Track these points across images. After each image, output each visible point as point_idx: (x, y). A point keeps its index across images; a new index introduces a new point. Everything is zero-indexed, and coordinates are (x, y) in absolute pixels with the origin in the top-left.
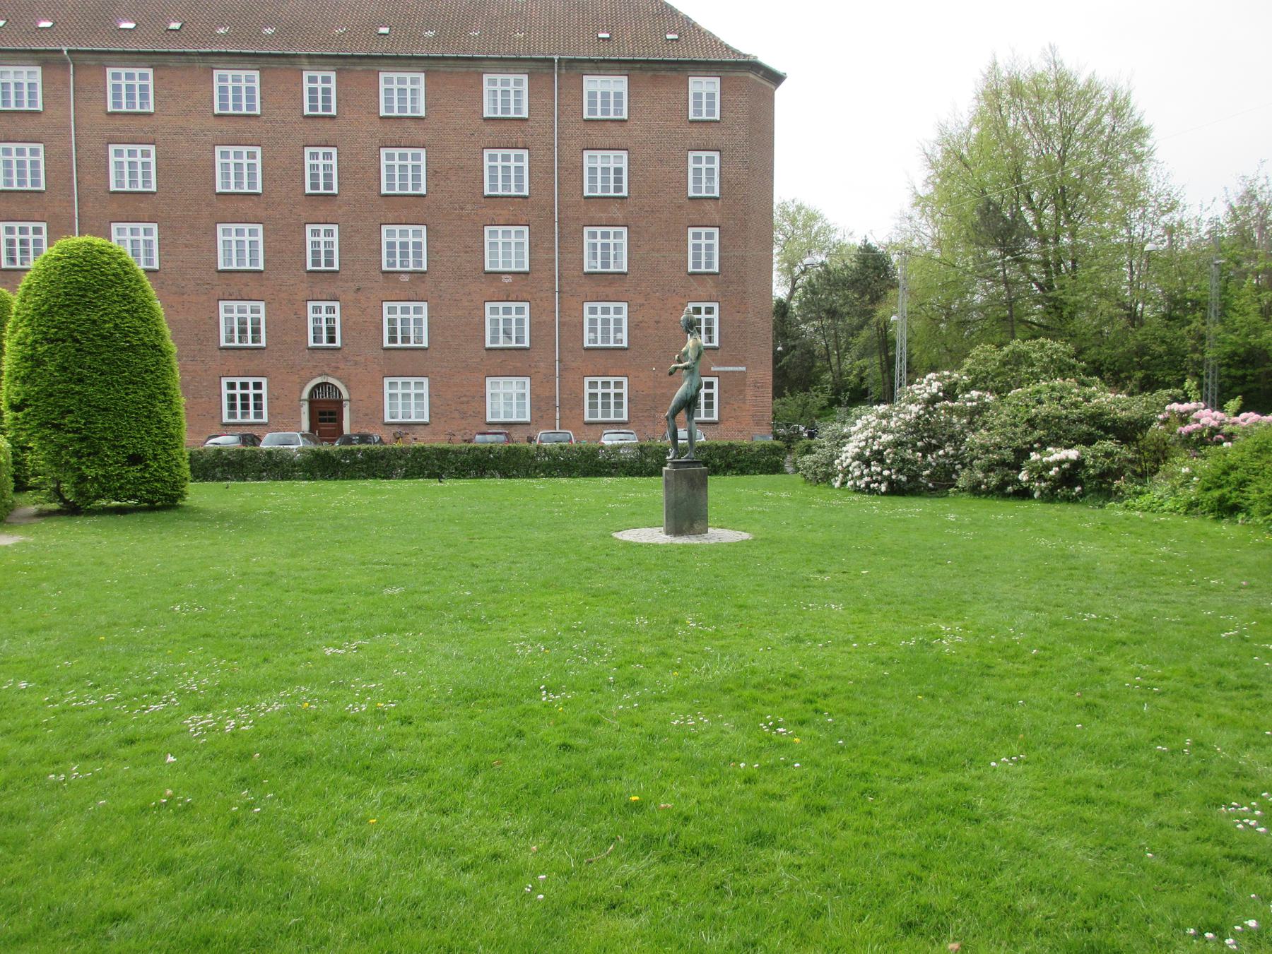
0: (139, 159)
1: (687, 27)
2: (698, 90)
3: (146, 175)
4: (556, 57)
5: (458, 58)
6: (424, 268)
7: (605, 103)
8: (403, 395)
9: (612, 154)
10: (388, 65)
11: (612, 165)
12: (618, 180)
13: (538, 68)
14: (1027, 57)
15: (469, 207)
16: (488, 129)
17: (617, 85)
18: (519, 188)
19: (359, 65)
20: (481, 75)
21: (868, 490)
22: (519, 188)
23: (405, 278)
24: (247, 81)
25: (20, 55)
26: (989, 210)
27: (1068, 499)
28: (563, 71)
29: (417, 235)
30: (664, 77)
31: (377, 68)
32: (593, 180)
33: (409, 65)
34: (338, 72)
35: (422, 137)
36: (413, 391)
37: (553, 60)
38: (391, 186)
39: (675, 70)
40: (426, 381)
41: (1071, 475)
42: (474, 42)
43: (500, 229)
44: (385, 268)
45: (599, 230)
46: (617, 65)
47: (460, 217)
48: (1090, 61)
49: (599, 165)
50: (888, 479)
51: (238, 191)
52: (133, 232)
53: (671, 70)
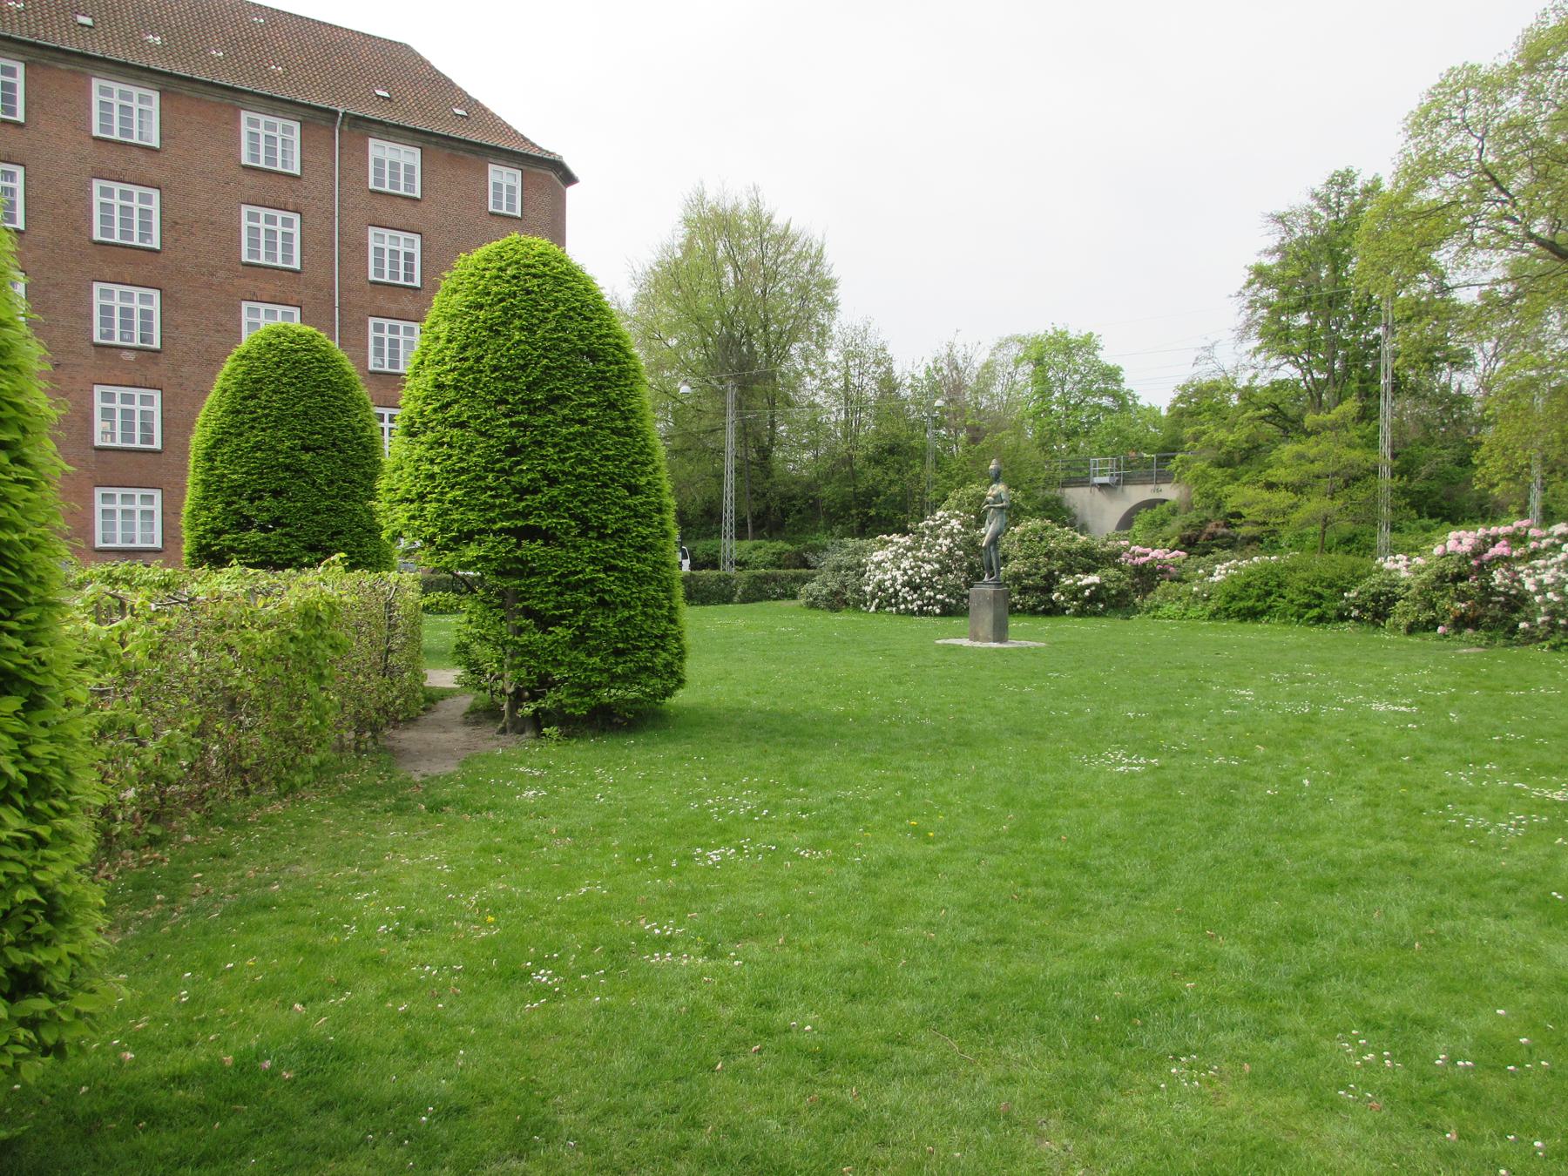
0: (279, 228)
1: (476, 111)
2: (498, 180)
3: (288, 248)
4: (341, 110)
5: (212, 84)
6: (157, 345)
7: (394, 176)
8: (124, 512)
9: (402, 235)
10: (106, 71)
11: (402, 249)
12: (409, 268)
13: (315, 119)
14: (730, 188)
15: (222, 274)
16: (248, 180)
17: (408, 156)
18: (288, 258)
19: (62, 61)
20: (237, 110)
21: (921, 612)
22: (288, 258)
23: (131, 356)
24: (141, 101)
25: (99, 64)
26: (729, 344)
27: (1095, 614)
28: (346, 128)
29: (146, 303)
30: (44, 66)
31: (89, 71)
32: (379, 262)
33: (139, 78)
34: (28, 65)
35: (155, 174)
36: (138, 506)
37: (336, 113)
38: (107, 231)
39: (474, 153)
40: (157, 494)
41: (1098, 594)
42: (81, 28)
43: (263, 307)
44: (97, 339)
45: (387, 323)
46: (411, 134)
47: (210, 286)
48: (790, 209)
49: (387, 246)
50: (942, 602)
51: (269, 263)
52: (123, 296)
53: (470, 152)
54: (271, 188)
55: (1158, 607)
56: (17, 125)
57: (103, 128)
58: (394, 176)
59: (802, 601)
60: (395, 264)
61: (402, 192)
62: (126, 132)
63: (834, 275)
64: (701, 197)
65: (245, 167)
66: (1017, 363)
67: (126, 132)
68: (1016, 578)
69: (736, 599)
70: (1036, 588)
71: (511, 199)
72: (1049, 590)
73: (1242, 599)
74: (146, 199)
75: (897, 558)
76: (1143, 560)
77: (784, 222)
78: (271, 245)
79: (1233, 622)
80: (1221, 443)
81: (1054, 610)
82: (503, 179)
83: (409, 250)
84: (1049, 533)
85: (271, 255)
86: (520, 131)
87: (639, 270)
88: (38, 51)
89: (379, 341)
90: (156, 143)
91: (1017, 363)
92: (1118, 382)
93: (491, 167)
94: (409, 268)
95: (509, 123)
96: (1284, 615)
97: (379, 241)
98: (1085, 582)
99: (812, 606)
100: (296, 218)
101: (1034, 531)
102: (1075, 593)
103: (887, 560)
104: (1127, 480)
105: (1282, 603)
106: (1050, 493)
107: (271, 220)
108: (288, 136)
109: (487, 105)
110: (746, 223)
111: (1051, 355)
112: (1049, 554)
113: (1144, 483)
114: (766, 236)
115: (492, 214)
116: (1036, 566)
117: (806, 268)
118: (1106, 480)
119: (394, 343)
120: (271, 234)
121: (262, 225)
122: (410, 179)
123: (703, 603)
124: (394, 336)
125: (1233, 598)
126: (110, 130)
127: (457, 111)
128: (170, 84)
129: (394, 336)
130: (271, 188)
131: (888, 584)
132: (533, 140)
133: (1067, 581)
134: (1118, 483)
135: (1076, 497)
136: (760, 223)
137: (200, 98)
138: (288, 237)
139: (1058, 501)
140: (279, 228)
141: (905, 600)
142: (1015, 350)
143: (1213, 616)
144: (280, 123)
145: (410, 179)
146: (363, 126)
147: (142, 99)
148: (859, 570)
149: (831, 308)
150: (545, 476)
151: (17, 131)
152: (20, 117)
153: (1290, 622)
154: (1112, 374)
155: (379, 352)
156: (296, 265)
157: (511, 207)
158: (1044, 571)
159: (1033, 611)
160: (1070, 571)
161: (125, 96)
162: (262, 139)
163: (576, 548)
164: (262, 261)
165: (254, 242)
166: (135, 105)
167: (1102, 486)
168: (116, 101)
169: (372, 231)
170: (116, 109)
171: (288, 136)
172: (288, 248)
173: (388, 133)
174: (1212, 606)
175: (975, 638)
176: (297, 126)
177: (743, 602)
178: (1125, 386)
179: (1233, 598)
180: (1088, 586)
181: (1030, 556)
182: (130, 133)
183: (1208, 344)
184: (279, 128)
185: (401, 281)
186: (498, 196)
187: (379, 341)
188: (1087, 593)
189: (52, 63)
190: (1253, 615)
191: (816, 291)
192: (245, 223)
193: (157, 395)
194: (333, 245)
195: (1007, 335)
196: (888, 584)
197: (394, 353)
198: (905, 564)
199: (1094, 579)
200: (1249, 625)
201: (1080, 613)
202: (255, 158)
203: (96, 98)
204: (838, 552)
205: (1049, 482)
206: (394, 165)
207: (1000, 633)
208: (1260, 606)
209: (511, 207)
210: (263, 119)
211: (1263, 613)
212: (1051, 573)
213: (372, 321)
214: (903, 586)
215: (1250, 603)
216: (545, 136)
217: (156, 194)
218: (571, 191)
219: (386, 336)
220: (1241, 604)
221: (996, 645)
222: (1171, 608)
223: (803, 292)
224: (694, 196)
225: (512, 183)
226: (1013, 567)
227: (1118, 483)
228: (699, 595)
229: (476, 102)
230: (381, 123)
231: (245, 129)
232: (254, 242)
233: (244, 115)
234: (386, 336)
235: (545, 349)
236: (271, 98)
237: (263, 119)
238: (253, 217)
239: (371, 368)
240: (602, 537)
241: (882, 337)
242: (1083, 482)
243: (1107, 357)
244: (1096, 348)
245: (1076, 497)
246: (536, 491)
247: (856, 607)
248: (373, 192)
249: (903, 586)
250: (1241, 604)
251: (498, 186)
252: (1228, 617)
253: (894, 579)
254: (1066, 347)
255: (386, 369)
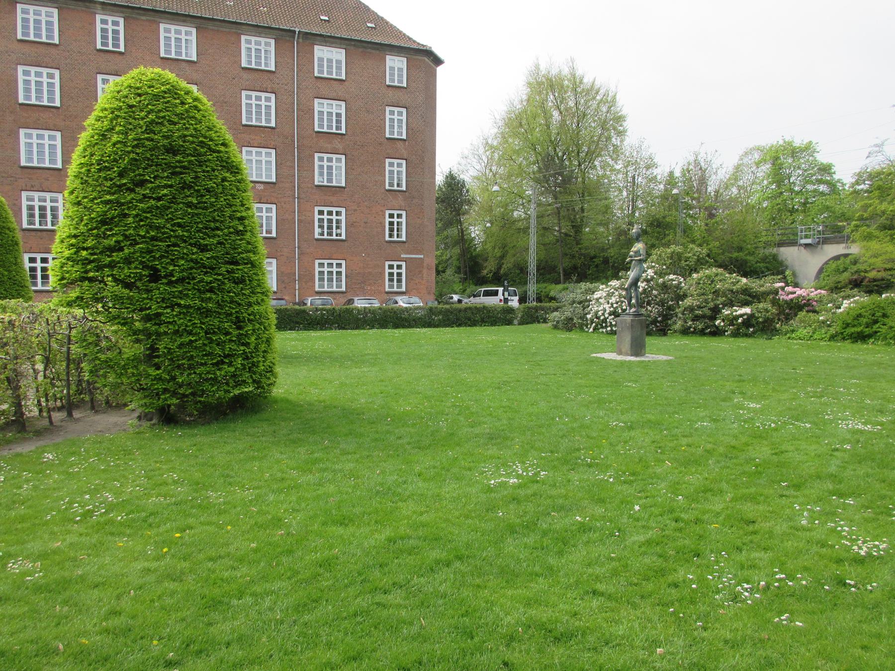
1: (382, 24)
3: (268, 114)
4: (297, 30)
5: (224, 21)
7: (330, 67)
9: (334, 103)
10: (167, 19)
11: (334, 111)
13: (283, 36)
14: (556, 63)
16: (245, 75)
17: (338, 54)
18: (268, 120)
19: (144, 15)
20: (239, 35)
22: (268, 120)
27: (746, 335)
28: (301, 40)
30: (134, 18)
31: (158, 20)
32: (321, 120)
37: (295, 32)
41: (749, 321)
43: (254, 150)
45: (325, 156)
48: (595, 71)
49: (325, 110)
53: (374, 49)
54: (259, 80)
55: (793, 331)
56: (120, 53)
57: (103, 44)
58: (330, 67)
59: (550, 324)
60: (330, 120)
61: (334, 76)
62: (178, 53)
63: (623, 112)
64: (537, 67)
65: (243, 68)
66: (758, 165)
67: (178, 53)
68: (691, 309)
69: (516, 322)
70: (704, 316)
71: (400, 76)
72: (714, 318)
73: (854, 326)
74: (400, 114)
75: (610, 295)
76: (791, 296)
77: (591, 80)
78: (259, 113)
79: (847, 344)
80: (884, 212)
81: (717, 333)
82: (396, 64)
83: (339, 111)
84: (719, 278)
85: (259, 119)
86: (408, 34)
87: (498, 117)
88: (130, 10)
89: (321, 167)
90: (194, 58)
91: (758, 165)
92: (830, 174)
93: (388, 57)
94: (338, 122)
95: (401, 29)
96: (885, 338)
97: (321, 106)
98: (738, 313)
99: (556, 327)
100: (273, 96)
101: (708, 277)
102: (732, 320)
103: (605, 297)
104: (826, 241)
105: (884, 330)
106: (767, 252)
107: (258, 98)
108: (268, 48)
109: (388, 20)
110: (566, 82)
111: (781, 160)
112: (716, 293)
113: (838, 243)
114: (579, 90)
115: (389, 86)
116: (706, 301)
117: (604, 109)
118: (809, 241)
119: (330, 168)
120: (39, 84)
121: (254, 102)
122: (339, 68)
123: (492, 325)
124: (330, 164)
125: (848, 325)
126: (28, 35)
127: (369, 25)
128: (201, 23)
129: (330, 164)
130: (259, 80)
131: (600, 313)
132: (414, 39)
133: (726, 312)
134: (818, 243)
135: (788, 253)
136: (576, 83)
137: (294, 41)
138: (268, 108)
139: (775, 257)
140: (263, 103)
141: (611, 325)
142: (757, 156)
143: (832, 338)
144: (263, 40)
145: (339, 68)
146: (311, 39)
147: (187, 33)
148: (584, 303)
149: (621, 134)
150: (126, 237)
151: (121, 57)
152: (122, 49)
153: (889, 344)
154: (826, 169)
155: (321, 174)
156: (273, 124)
157: (400, 81)
158: (711, 305)
159: (702, 333)
160: (731, 304)
161: (178, 32)
162: (253, 50)
163: (148, 291)
164: (254, 123)
165: (249, 112)
166: (183, 37)
167: (807, 246)
168: (173, 35)
169: (316, 101)
170: (173, 40)
171: (268, 48)
172: (268, 114)
173: (326, 42)
174: (832, 331)
175: (620, 353)
176: (273, 42)
177: (521, 323)
178: (836, 177)
179: (848, 325)
180: (741, 316)
181: (703, 294)
182: (180, 54)
183: (878, 142)
184: (263, 44)
185: (334, 131)
186: (392, 75)
187: (321, 167)
188: (740, 320)
189: (138, 17)
190: (861, 338)
191: (613, 123)
192: (244, 101)
193: (274, 207)
194: (296, 112)
195: (751, 146)
196: (600, 313)
197: (330, 174)
198: (613, 300)
199: (747, 310)
200: (860, 346)
201: (736, 334)
202: (250, 62)
203: (162, 35)
204: (569, 293)
205: (767, 244)
206: (330, 61)
207: (638, 348)
208: (867, 331)
209: (400, 81)
210: (253, 39)
211: (869, 336)
212: (716, 306)
213: (317, 155)
214: (610, 314)
215: (859, 329)
216: (421, 36)
217: (404, 111)
218: (440, 70)
219: (325, 164)
220: (853, 330)
221: (633, 358)
222: (803, 332)
223: (604, 125)
224: (533, 68)
225: (401, 66)
226: (688, 302)
227: (818, 243)
228: (295, 320)
229: (382, 18)
230: (321, 35)
231: (244, 46)
232: (249, 112)
233: (243, 38)
234: (325, 164)
235: (133, 147)
236: (257, 26)
237: (253, 39)
238: (249, 97)
239: (316, 183)
240: (170, 283)
241: (650, 151)
242: (793, 243)
243: (822, 158)
244: (814, 152)
245: (788, 253)
246: (121, 249)
247: (581, 327)
248: (317, 78)
249: (610, 314)
250: (853, 330)
251: (321, 60)
252: (844, 339)
253: (605, 310)
254: (794, 152)
255: (325, 183)
